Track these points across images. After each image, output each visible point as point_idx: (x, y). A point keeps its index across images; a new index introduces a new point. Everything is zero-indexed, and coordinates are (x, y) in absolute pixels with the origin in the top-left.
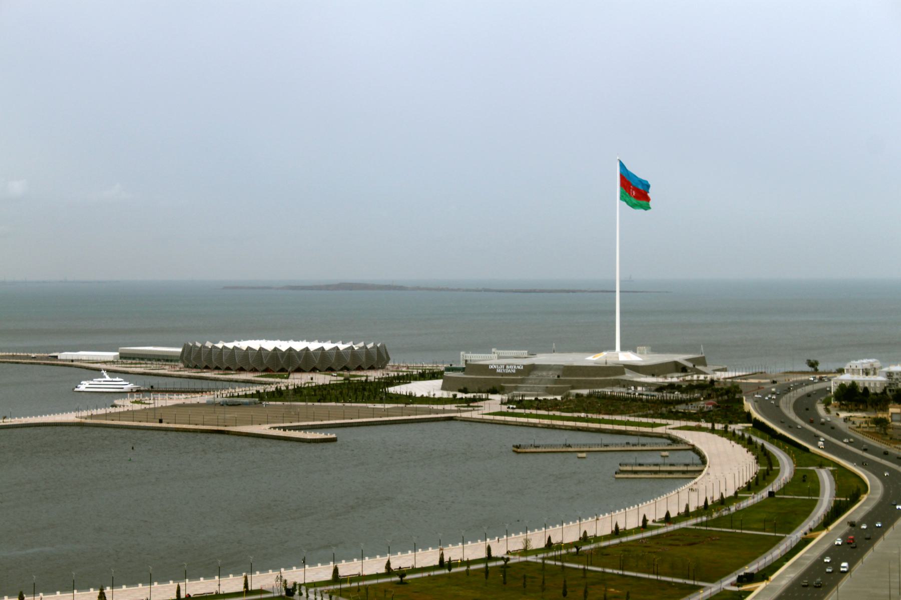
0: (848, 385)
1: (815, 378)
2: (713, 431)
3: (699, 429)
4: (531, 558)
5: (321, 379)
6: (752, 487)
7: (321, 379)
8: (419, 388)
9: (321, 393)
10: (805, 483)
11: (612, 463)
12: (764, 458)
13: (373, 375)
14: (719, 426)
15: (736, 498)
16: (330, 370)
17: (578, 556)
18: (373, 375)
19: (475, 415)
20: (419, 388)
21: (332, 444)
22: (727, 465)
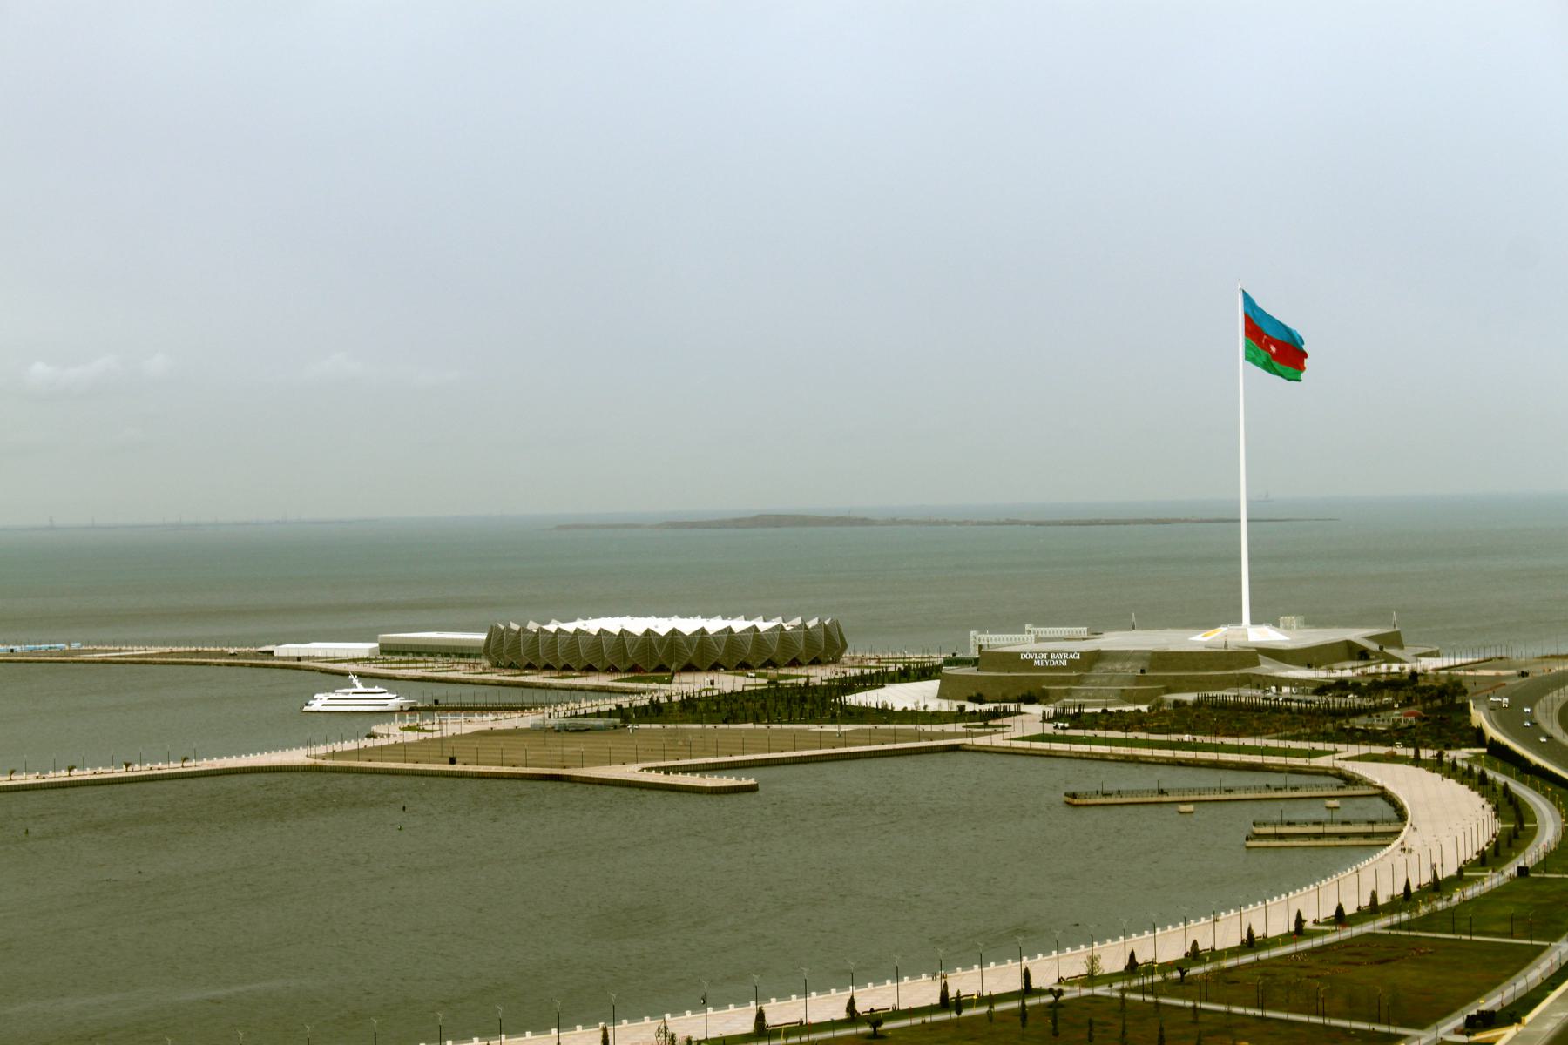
2: (1417, 761)
3: (1393, 759)
4: (1101, 990)
5: (728, 683)
7: (728, 683)
8: (899, 696)
12: (1508, 806)
13: (819, 675)
14: (1427, 754)
15: (1460, 879)
16: (744, 666)
17: (1184, 985)
18: (819, 675)
19: (998, 741)
20: (899, 696)
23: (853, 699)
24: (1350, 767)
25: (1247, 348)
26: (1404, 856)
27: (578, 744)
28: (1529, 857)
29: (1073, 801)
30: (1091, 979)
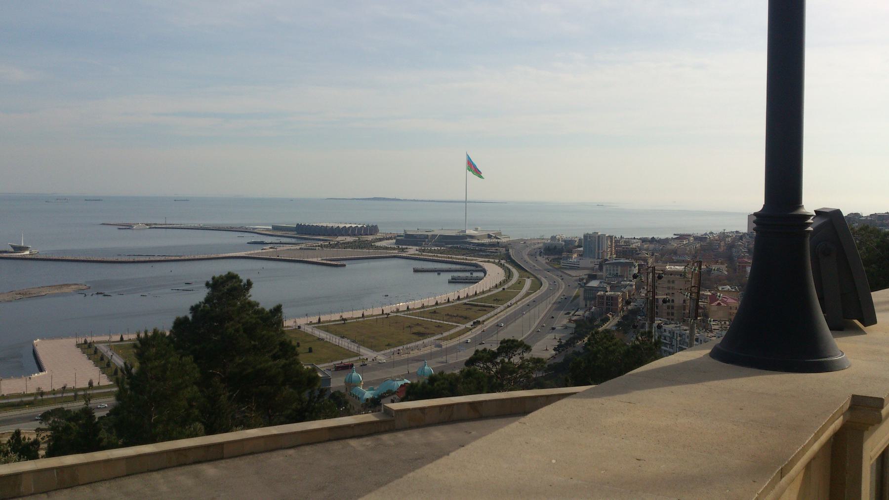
0: (866, 433)
1: (856, 239)
2: (494, 263)
3: (488, 262)
4: (401, 314)
5: (349, 239)
6: (505, 282)
7: (349, 239)
8: (384, 243)
9: (346, 245)
10: (520, 284)
11: (449, 276)
12: (509, 275)
13: (370, 238)
14: (497, 261)
15: (490, 290)
16: (354, 235)
17: (421, 314)
18: (370, 238)
19: (404, 255)
20: (384, 243)
21: (342, 268)
22: (494, 274)
23: (378, 244)
24: (481, 264)
25: (814, 458)
26: (301, 344)
27: (310, 252)
28: (510, 284)
29: (416, 271)
30: (398, 311)
